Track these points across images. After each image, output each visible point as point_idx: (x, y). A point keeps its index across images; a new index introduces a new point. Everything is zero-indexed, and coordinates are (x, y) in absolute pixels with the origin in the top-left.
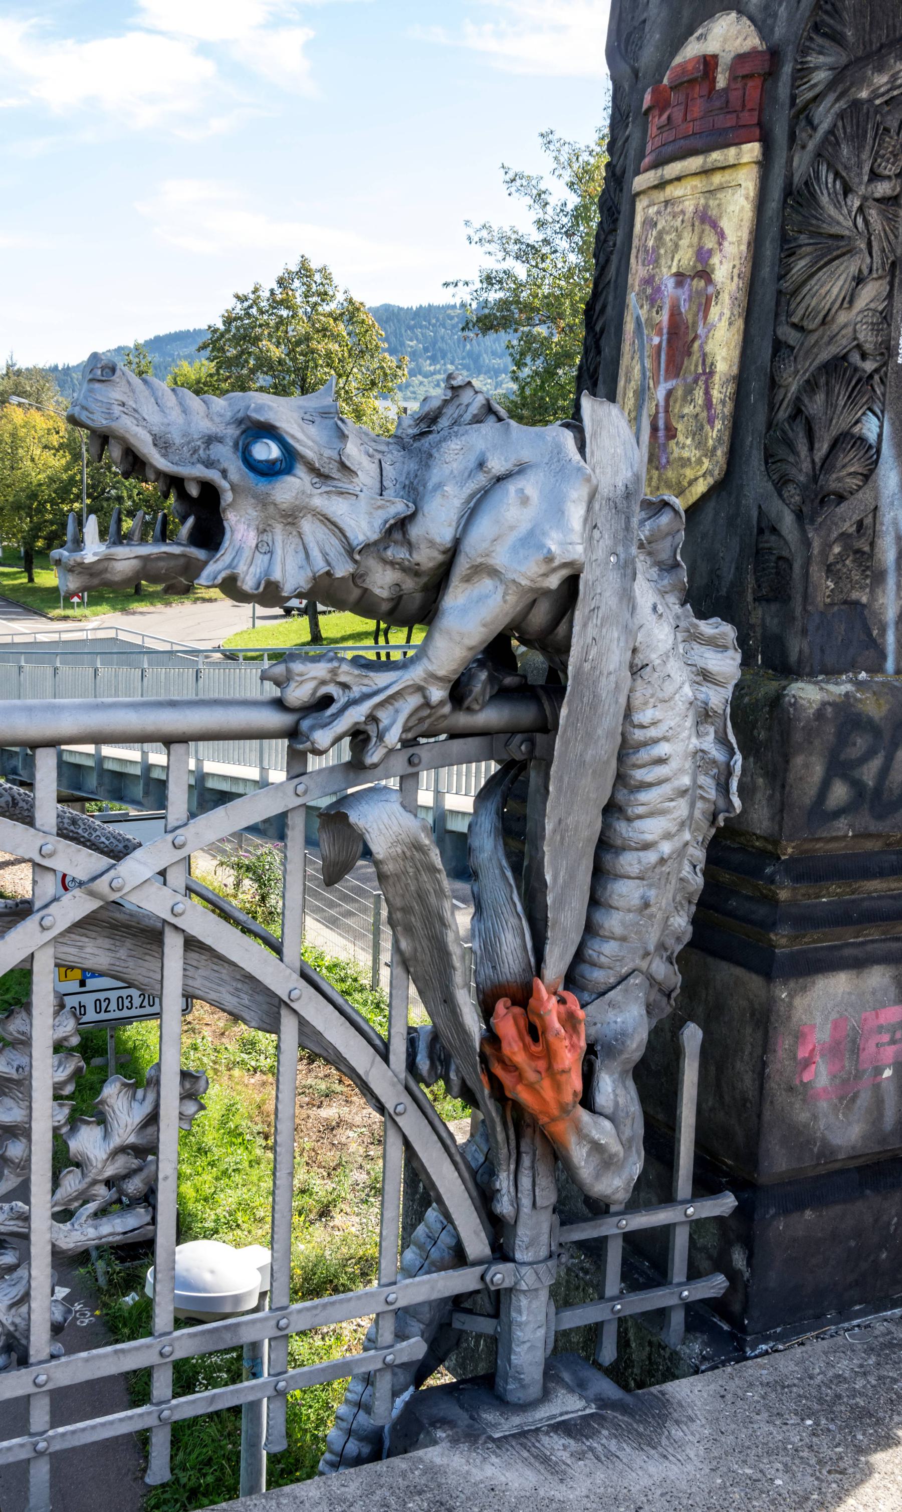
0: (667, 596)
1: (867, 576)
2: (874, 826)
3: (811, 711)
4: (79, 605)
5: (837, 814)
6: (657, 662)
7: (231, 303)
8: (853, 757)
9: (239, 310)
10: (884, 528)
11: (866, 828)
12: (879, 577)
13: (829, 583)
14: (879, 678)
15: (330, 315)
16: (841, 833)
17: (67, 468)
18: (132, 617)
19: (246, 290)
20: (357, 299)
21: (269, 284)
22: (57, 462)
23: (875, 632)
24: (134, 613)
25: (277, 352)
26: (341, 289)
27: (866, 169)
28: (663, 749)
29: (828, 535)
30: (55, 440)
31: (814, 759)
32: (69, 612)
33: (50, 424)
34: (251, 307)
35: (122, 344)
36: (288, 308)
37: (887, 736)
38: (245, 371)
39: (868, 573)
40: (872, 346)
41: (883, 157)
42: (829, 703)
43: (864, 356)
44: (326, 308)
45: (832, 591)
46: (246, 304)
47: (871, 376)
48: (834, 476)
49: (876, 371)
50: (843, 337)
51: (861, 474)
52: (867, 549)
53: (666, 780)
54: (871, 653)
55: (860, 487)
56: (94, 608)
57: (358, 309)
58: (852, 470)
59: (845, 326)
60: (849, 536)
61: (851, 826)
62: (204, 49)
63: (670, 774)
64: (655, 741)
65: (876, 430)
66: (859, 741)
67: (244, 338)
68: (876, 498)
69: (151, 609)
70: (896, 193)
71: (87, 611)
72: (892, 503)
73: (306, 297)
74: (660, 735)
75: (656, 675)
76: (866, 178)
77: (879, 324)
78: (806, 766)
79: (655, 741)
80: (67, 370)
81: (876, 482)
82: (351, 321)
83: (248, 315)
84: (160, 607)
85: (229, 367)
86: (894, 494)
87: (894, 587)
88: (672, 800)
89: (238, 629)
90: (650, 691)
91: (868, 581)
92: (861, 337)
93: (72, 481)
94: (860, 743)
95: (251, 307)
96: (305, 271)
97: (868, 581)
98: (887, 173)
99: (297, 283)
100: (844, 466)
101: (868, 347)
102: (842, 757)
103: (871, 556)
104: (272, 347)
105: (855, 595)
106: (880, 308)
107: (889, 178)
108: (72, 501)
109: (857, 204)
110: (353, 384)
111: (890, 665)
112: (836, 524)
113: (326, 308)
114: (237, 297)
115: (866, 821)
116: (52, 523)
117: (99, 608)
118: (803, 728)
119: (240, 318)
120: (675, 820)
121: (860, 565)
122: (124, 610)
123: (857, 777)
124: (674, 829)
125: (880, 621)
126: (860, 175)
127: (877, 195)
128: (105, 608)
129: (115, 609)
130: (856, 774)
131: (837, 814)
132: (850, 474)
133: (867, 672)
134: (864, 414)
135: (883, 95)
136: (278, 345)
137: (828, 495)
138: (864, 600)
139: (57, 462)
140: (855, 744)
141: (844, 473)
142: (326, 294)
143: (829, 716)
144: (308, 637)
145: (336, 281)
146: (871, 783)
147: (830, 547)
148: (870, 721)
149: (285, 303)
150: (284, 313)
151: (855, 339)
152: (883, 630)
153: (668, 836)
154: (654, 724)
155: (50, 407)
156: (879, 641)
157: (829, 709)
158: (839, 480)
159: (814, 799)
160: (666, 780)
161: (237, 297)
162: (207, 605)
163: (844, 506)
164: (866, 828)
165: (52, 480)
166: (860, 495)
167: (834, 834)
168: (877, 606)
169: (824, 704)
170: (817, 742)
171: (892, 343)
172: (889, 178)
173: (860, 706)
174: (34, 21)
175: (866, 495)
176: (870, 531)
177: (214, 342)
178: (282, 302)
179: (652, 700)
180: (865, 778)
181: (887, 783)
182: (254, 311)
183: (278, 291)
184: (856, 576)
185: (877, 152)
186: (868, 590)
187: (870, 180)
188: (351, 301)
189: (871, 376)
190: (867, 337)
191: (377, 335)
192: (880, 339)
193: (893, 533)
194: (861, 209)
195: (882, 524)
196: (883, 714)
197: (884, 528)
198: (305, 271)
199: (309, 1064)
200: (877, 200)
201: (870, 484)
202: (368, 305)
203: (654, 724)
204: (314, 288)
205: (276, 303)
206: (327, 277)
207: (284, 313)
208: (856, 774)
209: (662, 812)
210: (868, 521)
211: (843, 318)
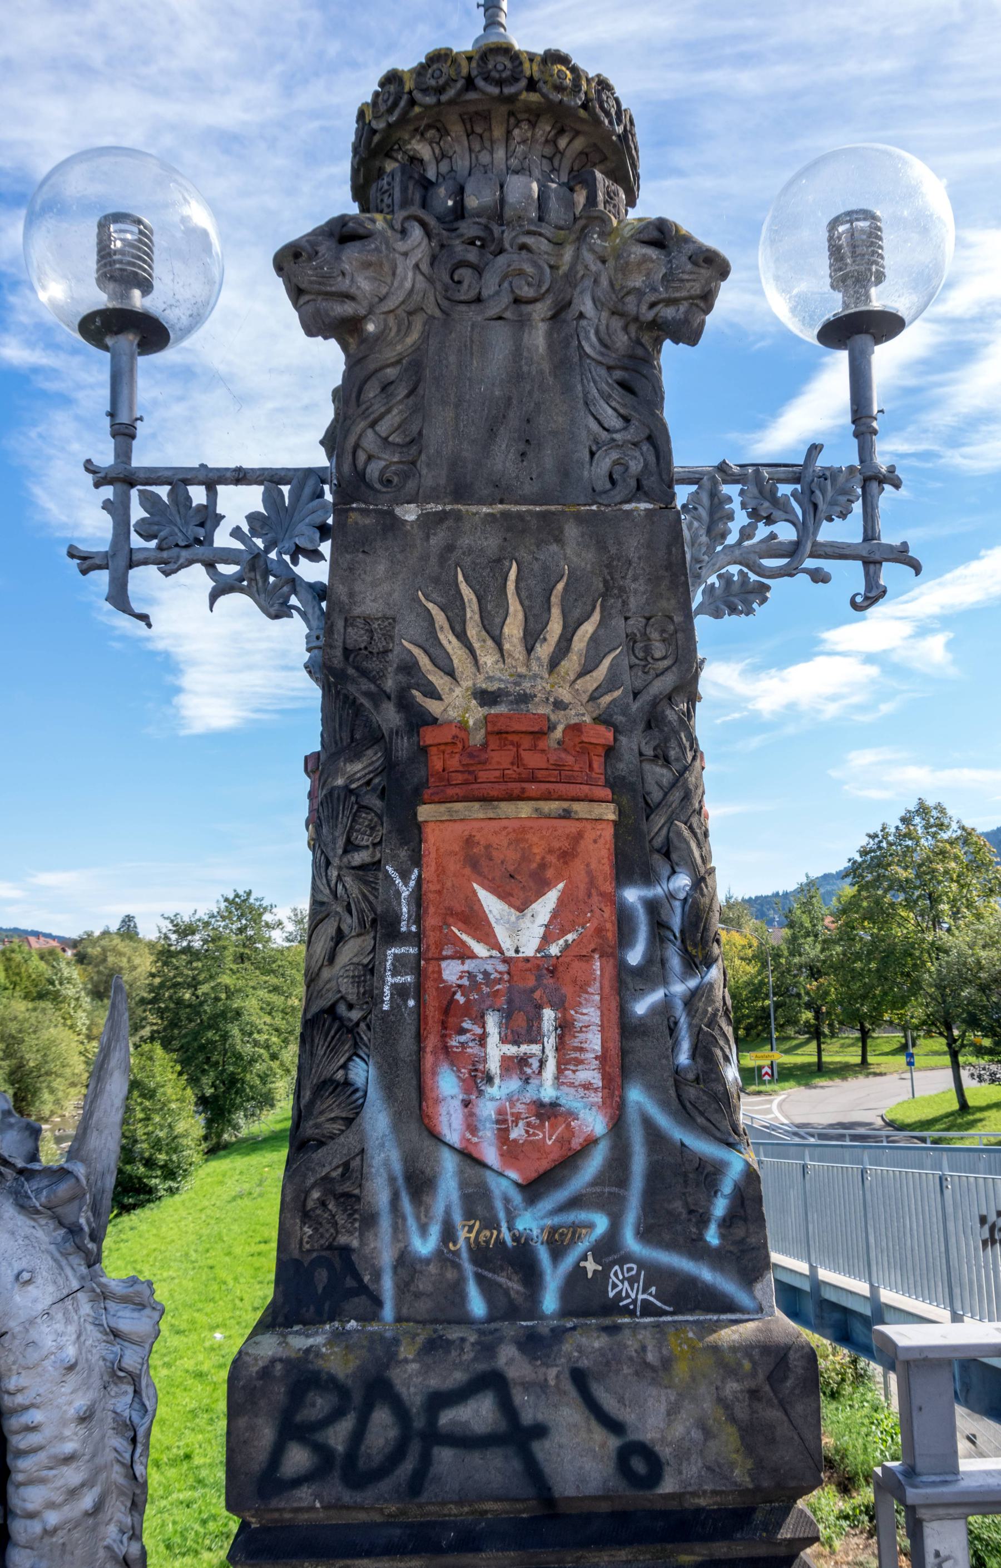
0: (71, 1258)
1: (355, 1220)
2: (347, 1497)
3: (255, 1369)
4: (770, 1082)
5: (297, 1482)
6: (17, 1329)
7: (864, 841)
8: (313, 1418)
9: (872, 844)
10: (373, 1170)
11: (339, 1499)
12: (370, 1220)
13: (306, 1229)
14: (374, 1327)
15: (947, 841)
16: (304, 1504)
17: (759, 973)
18: (813, 1091)
19: (877, 829)
20: (968, 824)
21: (894, 822)
22: (752, 969)
23: (366, 1279)
24: (815, 1087)
25: (903, 874)
26: (954, 819)
27: (341, 843)
28: (36, 1416)
29: (304, 1182)
30: (749, 953)
31: (260, 1421)
32: (762, 1088)
33: (745, 942)
34: (880, 842)
35: (827, 872)
36: (911, 839)
37: (357, 1398)
38: (880, 892)
39: (357, 1216)
40: (355, 997)
41: (358, 831)
42: (281, 1360)
43: (350, 1007)
44: (945, 836)
45: (310, 1237)
46: (877, 840)
47: (357, 1024)
48: (311, 1123)
49: (364, 1018)
50: (328, 990)
51: (342, 1119)
52: (357, 1192)
53: (40, 1448)
54: (361, 1302)
55: (342, 1131)
56: (782, 1084)
57: (970, 834)
58: (333, 1115)
59: (329, 981)
60: (332, 1180)
61: (317, 1496)
62: (870, 659)
63: (43, 1442)
64: (26, 1408)
65: (363, 1074)
66: (319, 1401)
67: (879, 865)
68: (362, 1141)
69: (831, 1083)
70: (376, 859)
71: (776, 1087)
72: (383, 1145)
73: (926, 828)
74: (27, 1402)
75: (17, 1342)
76: (340, 851)
77: (359, 977)
78: (252, 1428)
79: (26, 1408)
80: (786, 895)
81: (360, 1125)
82: (966, 842)
83: (880, 848)
84: (838, 1081)
85: (867, 890)
86: (384, 1135)
87: (390, 1230)
88: (51, 1468)
89: (900, 1099)
90: (11, 1359)
91: (357, 1225)
92: (343, 989)
93: (762, 983)
94: (319, 1405)
95: (880, 842)
96: (923, 810)
97: (357, 1225)
98: (364, 843)
99: (917, 820)
100: (322, 1113)
101: (352, 998)
102: (299, 1418)
103: (358, 1198)
104: (900, 870)
105: (343, 1239)
106: (366, 961)
107: (367, 847)
108: (764, 1000)
109: (335, 873)
110: (974, 893)
111: (388, 1312)
112: (313, 1170)
113: (945, 836)
114: (870, 836)
115: (335, 1489)
116: (748, 1017)
117: (787, 1084)
118: (244, 1387)
119: (874, 851)
120: (58, 1489)
121: (345, 1210)
122: (808, 1086)
123: (320, 1440)
124: (59, 1499)
125: (373, 1266)
126: (334, 849)
127: (355, 864)
128: (792, 1083)
129: (799, 1084)
130: (320, 1437)
131: (297, 1482)
132: (332, 1119)
133: (357, 1320)
134: (350, 1059)
135: (359, 779)
136: (906, 868)
137: (309, 1141)
138: (355, 1243)
139: (752, 969)
140: (313, 1405)
141: (322, 1119)
142: (942, 825)
143: (278, 1374)
144: (956, 1106)
145: (950, 812)
146: (340, 1448)
147: (307, 1193)
148: (332, 1379)
149: (908, 835)
150: (909, 843)
151: (339, 991)
152: (377, 1276)
153: (51, 1505)
154: (20, 1390)
155: (746, 931)
156: (372, 1287)
157: (279, 1366)
158: (317, 1126)
159: (264, 1465)
160: (40, 1448)
161: (870, 836)
162: (878, 1079)
163: (321, 1152)
164: (339, 1499)
165: (748, 984)
166: (342, 1139)
167: (295, 1505)
168: (367, 1250)
169: (273, 1361)
170: (262, 1403)
171: (376, 992)
172: (367, 847)
173: (321, 1362)
174: (747, 661)
175: (348, 1140)
176: (358, 1174)
177: (854, 871)
178: (905, 836)
179: (14, 1367)
180: (332, 1442)
181: (363, 1448)
182: (884, 844)
183: (902, 827)
184: (341, 1219)
185: (351, 827)
186: (357, 1234)
187: (346, 851)
188: (963, 828)
189: (357, 1024)
190: (349, 990)
191: (990, 852)
192: (362, 990)
193: (385, 1175)
194: (339, 878)
195: (370, 1166)
196: (349, 1371)
197: (373, 1170)
198: (923, 810)
199: (868, 1538)
200: (354, 868)
201: (354, 1127)
202: (979, 830)
203: (20, 1390)
204: (932, 821)
205: (901, 836)
206: (942, 811)
207: (909, 843)
208: (320, 1437)
209: (43, 1481)
210: (355, 1164)
211: (326, 974)
